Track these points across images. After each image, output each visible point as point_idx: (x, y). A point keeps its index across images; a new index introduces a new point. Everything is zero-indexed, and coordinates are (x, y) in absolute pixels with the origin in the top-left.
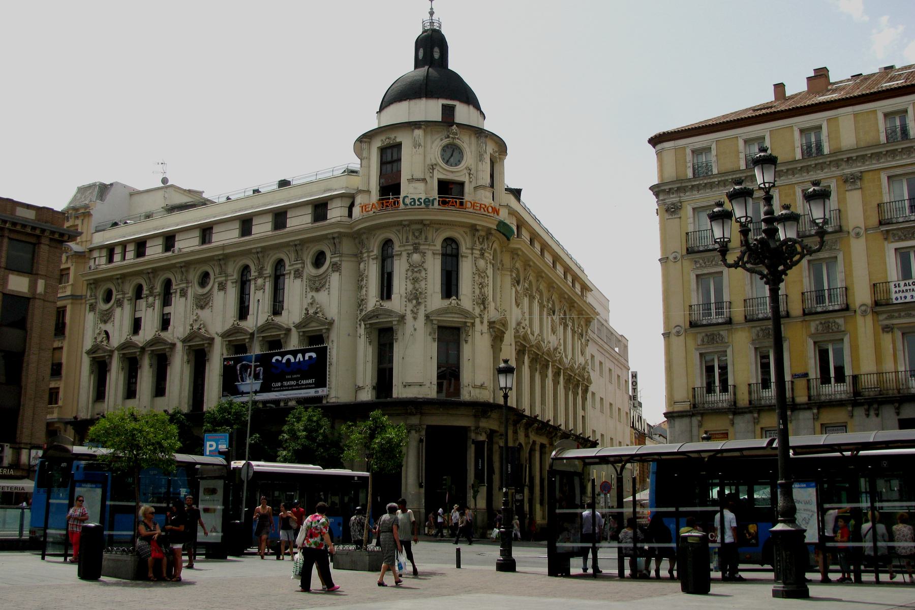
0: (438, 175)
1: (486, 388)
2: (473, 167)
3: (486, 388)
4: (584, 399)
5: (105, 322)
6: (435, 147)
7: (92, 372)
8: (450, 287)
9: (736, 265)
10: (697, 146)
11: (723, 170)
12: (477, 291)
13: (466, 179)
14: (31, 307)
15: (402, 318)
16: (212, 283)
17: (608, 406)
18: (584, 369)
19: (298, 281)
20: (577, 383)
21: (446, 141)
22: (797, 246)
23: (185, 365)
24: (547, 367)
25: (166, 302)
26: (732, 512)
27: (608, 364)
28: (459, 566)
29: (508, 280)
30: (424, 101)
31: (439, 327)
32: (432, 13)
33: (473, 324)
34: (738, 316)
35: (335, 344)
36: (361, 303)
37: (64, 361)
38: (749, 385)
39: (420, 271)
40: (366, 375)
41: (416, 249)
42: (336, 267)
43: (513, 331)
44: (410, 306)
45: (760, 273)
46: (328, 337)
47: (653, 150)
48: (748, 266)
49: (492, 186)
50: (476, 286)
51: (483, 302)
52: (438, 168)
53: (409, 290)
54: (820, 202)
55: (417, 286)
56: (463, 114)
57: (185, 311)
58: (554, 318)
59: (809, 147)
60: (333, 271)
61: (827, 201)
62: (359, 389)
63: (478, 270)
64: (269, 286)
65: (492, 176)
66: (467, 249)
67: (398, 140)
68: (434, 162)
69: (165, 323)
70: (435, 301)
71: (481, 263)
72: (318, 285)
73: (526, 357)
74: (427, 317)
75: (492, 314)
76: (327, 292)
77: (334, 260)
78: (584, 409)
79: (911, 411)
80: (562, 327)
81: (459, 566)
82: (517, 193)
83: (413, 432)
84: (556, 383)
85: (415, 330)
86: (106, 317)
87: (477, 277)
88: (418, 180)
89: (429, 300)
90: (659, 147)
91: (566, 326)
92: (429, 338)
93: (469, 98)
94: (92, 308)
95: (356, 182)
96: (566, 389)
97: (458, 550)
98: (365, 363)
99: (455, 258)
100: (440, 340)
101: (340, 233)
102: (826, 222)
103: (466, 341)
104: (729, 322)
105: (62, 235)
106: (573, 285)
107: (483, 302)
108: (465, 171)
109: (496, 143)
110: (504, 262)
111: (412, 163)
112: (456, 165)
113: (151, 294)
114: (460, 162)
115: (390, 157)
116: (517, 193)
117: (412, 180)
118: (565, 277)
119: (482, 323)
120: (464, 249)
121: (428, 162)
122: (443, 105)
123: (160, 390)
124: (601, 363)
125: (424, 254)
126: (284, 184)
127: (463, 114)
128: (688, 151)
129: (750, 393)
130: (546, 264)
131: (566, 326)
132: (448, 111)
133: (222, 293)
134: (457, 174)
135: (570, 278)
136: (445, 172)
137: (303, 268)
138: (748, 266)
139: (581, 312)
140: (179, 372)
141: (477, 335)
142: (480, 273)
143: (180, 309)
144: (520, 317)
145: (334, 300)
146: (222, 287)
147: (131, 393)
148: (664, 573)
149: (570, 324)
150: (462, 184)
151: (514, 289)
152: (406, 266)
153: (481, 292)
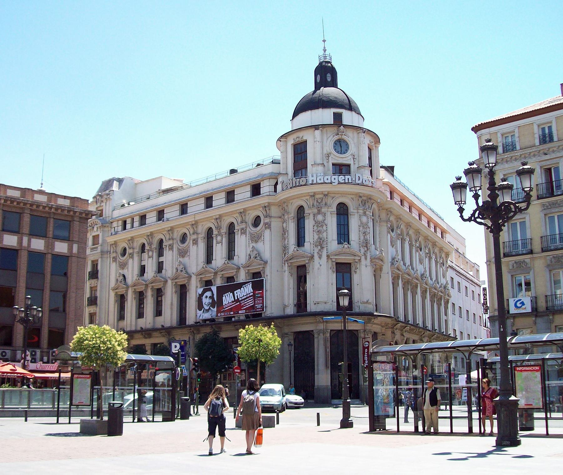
0: (331, 161)
2: (356, 154)
4: (446, 308)
5: (123, 269)
8: (343, 235)
9: (469, 220)
10: (505, 131)
11: (523, 146)
12: (362, 238)
13: (351, 162)
14: (70, 262)
15: (312, 257)
16: (189, 240)
18: (445, 287)
19: (243, 236)
20: (440, 298)
22: (512, 206)
23: (174, 294)
25: (161, 254)
27: (464, 283)
28: (318, 424)
29: (385, 229)
30: (320, 110)
31: (337, 263)
32: (325, 51)
33: (360, 260)
34: (537, 247)
35: (269, 277)
36: (285, 248)
37: (98, 295)
38: (546, 296)
39: (322, 226)
40: (290, 299)
41: (319, 212)
42: (268, 226)
44: (316, 250)
45: (485, 225)
46: (264, 273)
47: (476, 135)
48: (478, 220)
49: (370, 166)
50: (361, 235)
51: (366, 244)
52: (332, 156)
54: (528, 175)
56: (348, 117)
57: (173, 259)
58: (421, 253)
59: (544, 135)
61: (532, 175)
62: (285, 307)
63: (362, 223)
64: (225, 240)
65: (370, 159)
67: (304, 138)
69: (160, 267)
70: (333, 245)
71: (364, 219)
72: (256, 238)
74: (328, 256)
76: (262, 243)
77: (266, 221)
78: (446, 314)
79: (559, 319)
80: (427, 260)
81: (318, 424)
82: (390, 170)
83: (321, 334)
84: (424, 298)
85: (321, 265)
86: (123, 266)
87: (361, 228)
90: (479, 133)
91: (430, 258)
92: (330, 271)
93: (350, 106)
94: (115, 259)
95: (279, 168)
96: (432, 302)
97: (318, 414)
98: (289, 288)
99: (346, 216)
102: (531, 190)
103: (356, 272)
104: (531, 252)
108: (351, 157)
109: (371, 136)
110: (381, 217)
111: (313, 154)
112: (344, 153)
114: (347, 151)
115: (300, 151)
116: (390, 170)
117: (315, 164)
118: (429, 226)
119: (366, 259)
120: (351, 209)
121: (325, 152)
123: (158, 312)
126: (233, 171)
127: (348, 117)
128: (499, 135)
129: (547, 302)
130: (414, 218)
132: (338, 118)
133: (195, 247)
136: (337, 158)
138: (478, 220)
140: (170, 299)
141: (363, 267)
143: (169, 258)
144: (395, 253)
145: (268, 247)
148: (461, 426)
149: (434, 257)
150: (349, 166)
151: (389, 235)
153: (364, 238)
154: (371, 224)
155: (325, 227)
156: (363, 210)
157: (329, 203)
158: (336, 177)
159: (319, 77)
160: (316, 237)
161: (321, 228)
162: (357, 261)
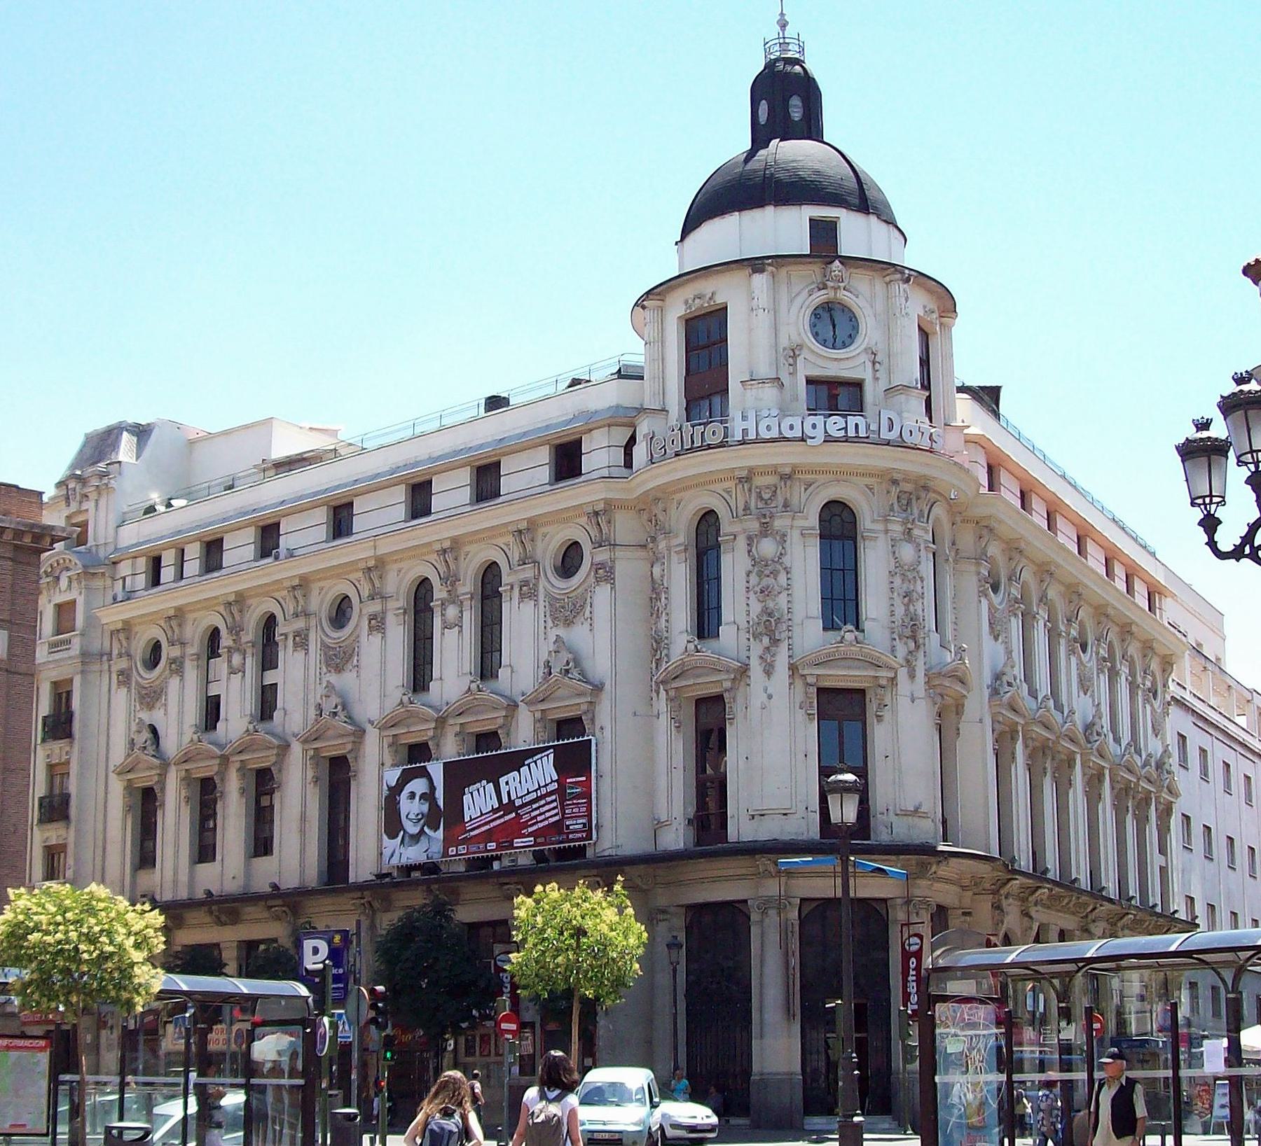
0: (803, 371)
1: (925, 816)
3: (925, 816)
4: (1164, 830)
6: (797, 304)
7: (129, 809)
8: (841, 603)
12: (900, 611)
13: (866, 374)
17: (1224, 841)
18: (1160, 765)
19: (528, 606)
20: (1143, 798)
21: (820, 297)
23: (310, 787)
24: (1071, 763)
25: (268, 661)
26: (198, 1104)
29: (970, 584)
30: (769, 210)
31: (821, 691)
32: (783, 25)
33: (893, 680)
37: (73, 789)
39: (775, 574)
42: (605, 573)
43: (987, 692)
44: (757, 649)
49: (926, 386)
50: (898, 601)
51: (912, 631)
52: (805, 353)
53: (753, 615)
55: (771, 605)
57: (306, 678)
60: (598, 580)
62: (658, 826)
63: (898, 565)
64: (470, 620)
65: (925, 362)
66: (873, 521)
67: (719, 300)
68: (796, 339)
69: (267, 702)
70: (809, 632)
72: (567, 612)
73: (1019, 746)
74: (793, 668)
75: (935, 653)
76: (587, 625)
77: (598, 559)
78: (1163, 850)
80: (1104, 679)
82: (989, 397)
84: (1093, 798)
85: (770, 697)
86: (150, 697)
87: (898, 581)
88: (763, 382)
89: (796, 631)
91: (1113, 674)
92: (800, 715)
93: (864, 199)
94: (125, 677)
95: (643, 394)
98: (670, 769)
99: (849, 543)
100: (822, 716)
101: (608, 502)
105: (37, 538)
106: (1130, 589)
107: (912, 631)
110: (960, 545)
112: (844, 346)
113: (237, 648)
115: (705, 340)
116: (989, 397)
117: (752, 380)
119: (912, 676)
120: (867, 522)
121: (784, 342)
122: (813, 222)
123: (262, 845)
124: (1203, 751)
125: (783, 538)
126: (495, 403)
131: (1113, 674)
132: (824, 234)
134: (844, 364)
135: (1119, 571)
137: (537, 578)
139: (1148, 647)
140: (298, 801)
141: (903, 702)
142: (903, 572)
143: (296, 674)
144: (1002, 658)
145: (605, 637)
146: (377, 624)
147: (205, 851)
149: (1124, 670)
150: (858, 385)
151: (984, 602)
152: (746, 563)
154: (927, 569)
155: (782, 578)
156: (904, 523)
157: (795, 501)
158: (819, 420)
159: (764, 107)
160: (756, 608)
161: (771, 581)
162: (883, 682)
